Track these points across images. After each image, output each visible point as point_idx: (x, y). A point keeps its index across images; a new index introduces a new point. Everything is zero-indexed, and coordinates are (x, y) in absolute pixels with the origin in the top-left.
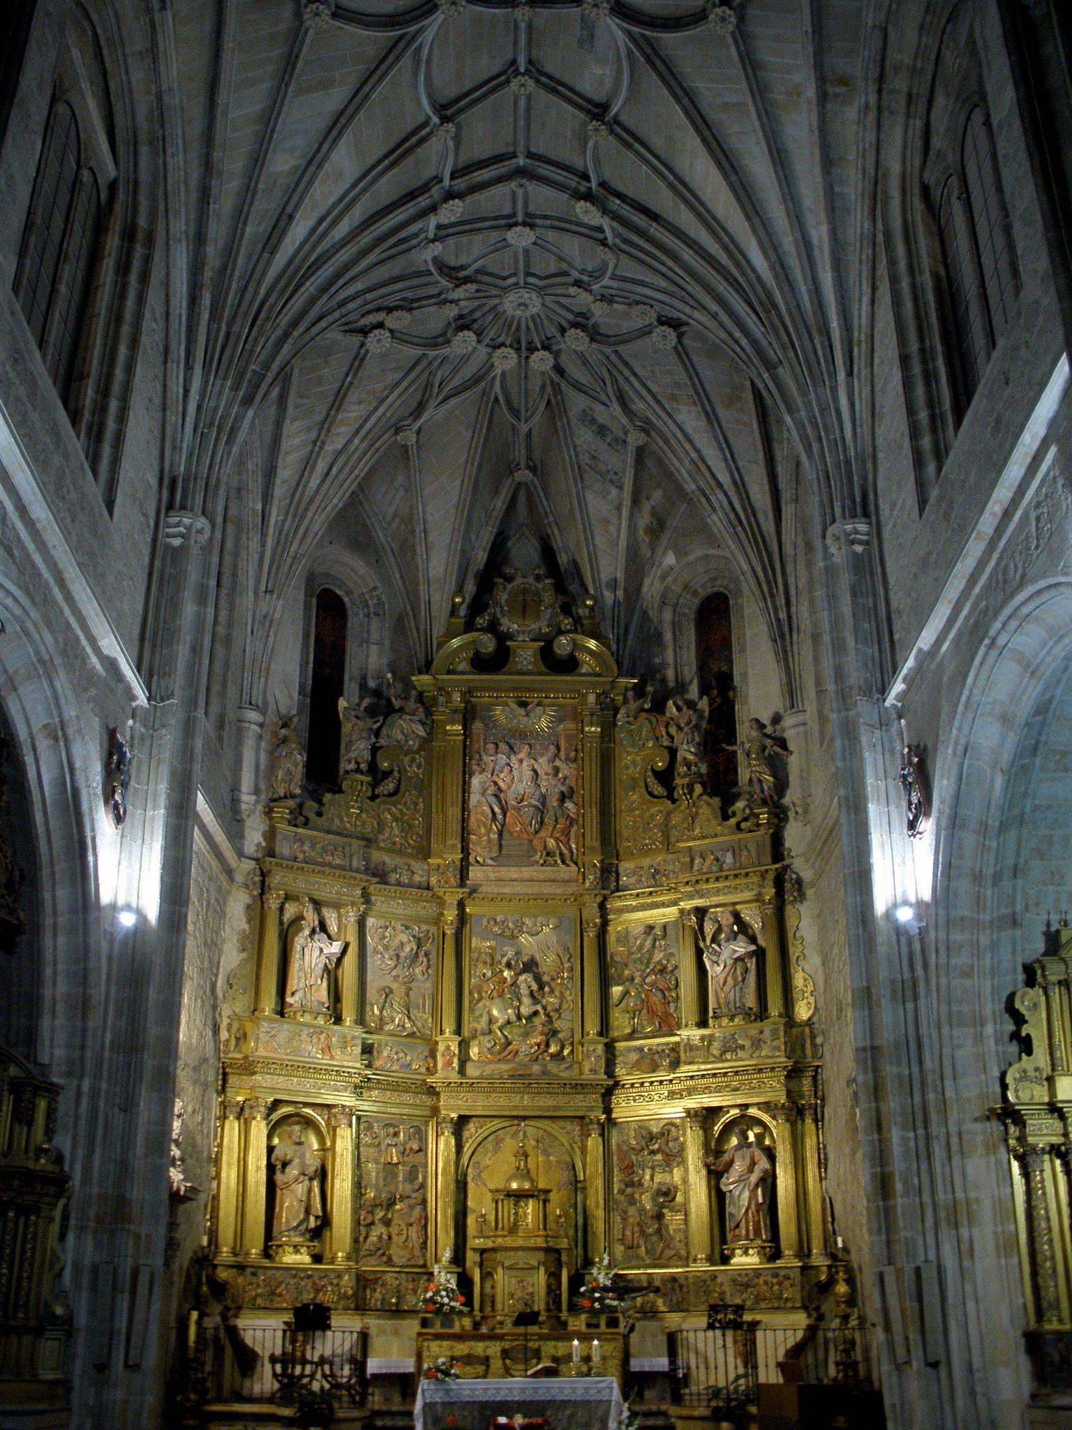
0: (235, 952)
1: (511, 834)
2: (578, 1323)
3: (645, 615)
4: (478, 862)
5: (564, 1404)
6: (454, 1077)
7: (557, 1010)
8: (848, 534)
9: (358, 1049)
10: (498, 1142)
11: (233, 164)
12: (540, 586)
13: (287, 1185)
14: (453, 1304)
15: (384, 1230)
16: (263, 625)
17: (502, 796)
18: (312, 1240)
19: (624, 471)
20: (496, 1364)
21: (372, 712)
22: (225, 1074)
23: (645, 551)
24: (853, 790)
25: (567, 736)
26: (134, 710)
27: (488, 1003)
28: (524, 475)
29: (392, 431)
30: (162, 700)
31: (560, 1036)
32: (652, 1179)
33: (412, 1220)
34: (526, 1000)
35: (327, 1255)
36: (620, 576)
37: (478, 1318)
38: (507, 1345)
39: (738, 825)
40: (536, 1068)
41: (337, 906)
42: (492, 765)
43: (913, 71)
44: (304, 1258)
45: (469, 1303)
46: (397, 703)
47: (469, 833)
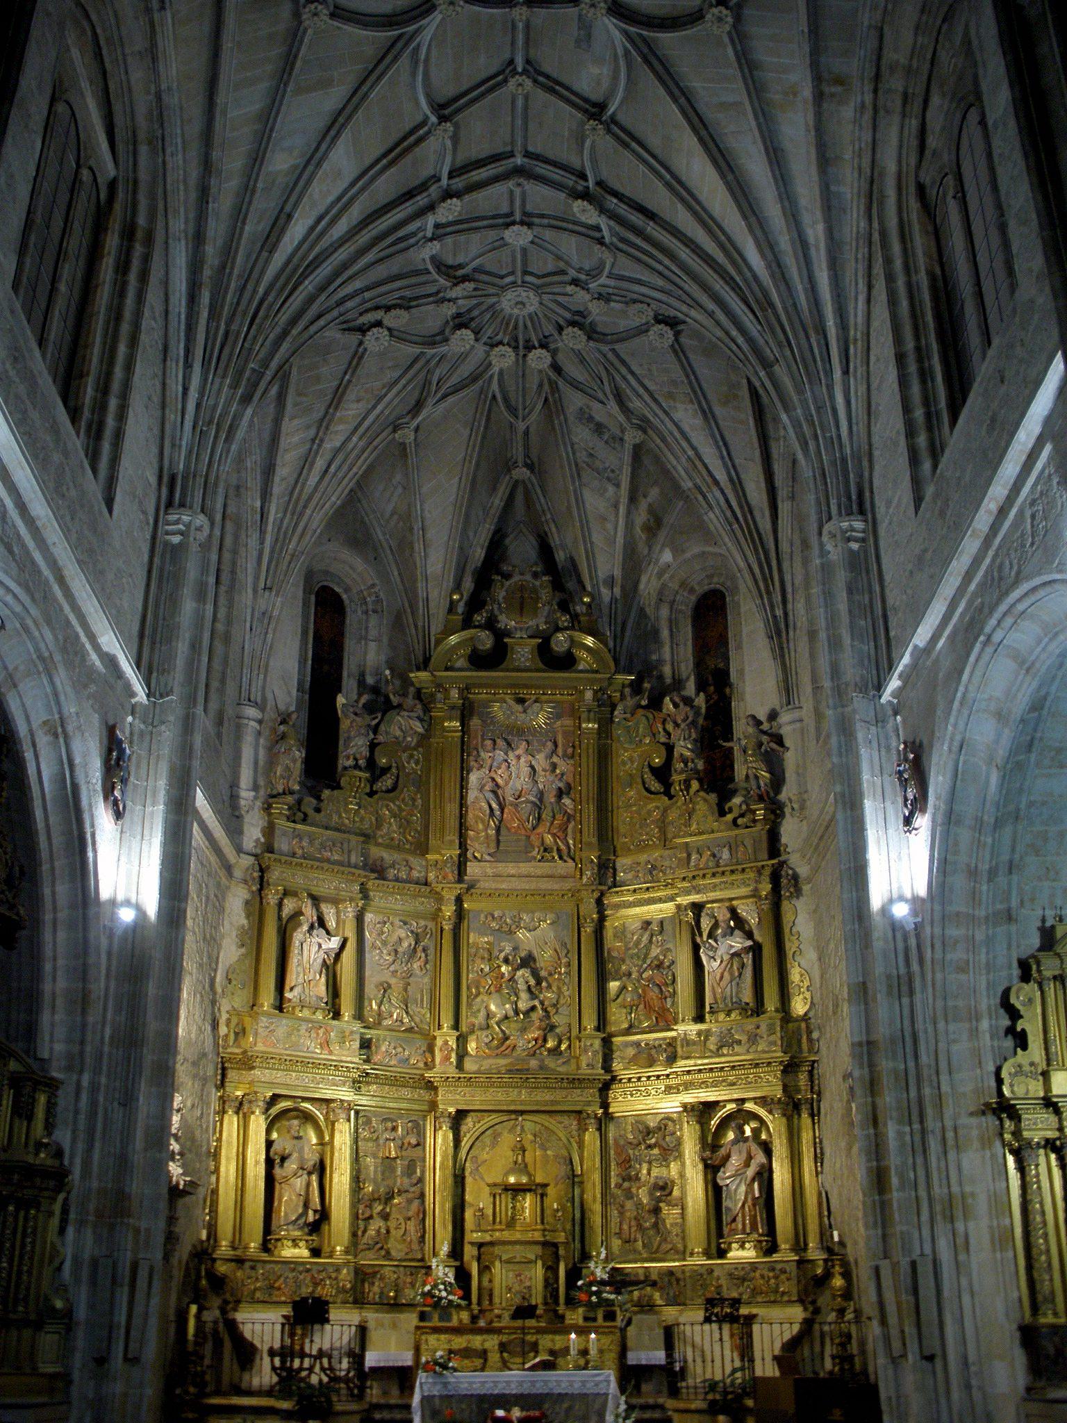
0: (234, 948)
1: (509, 829)
2: (575, 1316)
3: (642, 612)
4: (475, 857)
5: (561, 1397)
6: (452, 1072)
7: (554, 1005)
8: (844, 532)
9: (357, 1044)
10: (496, 1136)
11: (232, 163)
12: (537, 583)
13: (286, 1179)
14: (450, 1297)
15: (382, 1223)
16: (262, 622)
17: (500, 792)
18: (310, 1234)
19: (621, 469)
20: (494, 1357)
21: (370, 708)
22: (224, 1069)
23: (642, 548)
24: (849, 786)
25: (564, 733)
26: (134, 707)
27: (486, 998)
28: (521, 473)
29: (390, 428)
30: (162, 696)
31: (558, 1030)
32: (649, 1174)
33: (410, 1214)
34: (524, 995)
35: (326, 1249)
36: (617, 573)
37: (476, 1312)
38: (505, 1338)
39: (735, 821)
40: (534, 1063)
41: (335, 901)
42: (489, 761)
43: (909, 71)
44: (303, 1252)
45: (467, 1296)
46: (395, 700)
47: (467, 829)
